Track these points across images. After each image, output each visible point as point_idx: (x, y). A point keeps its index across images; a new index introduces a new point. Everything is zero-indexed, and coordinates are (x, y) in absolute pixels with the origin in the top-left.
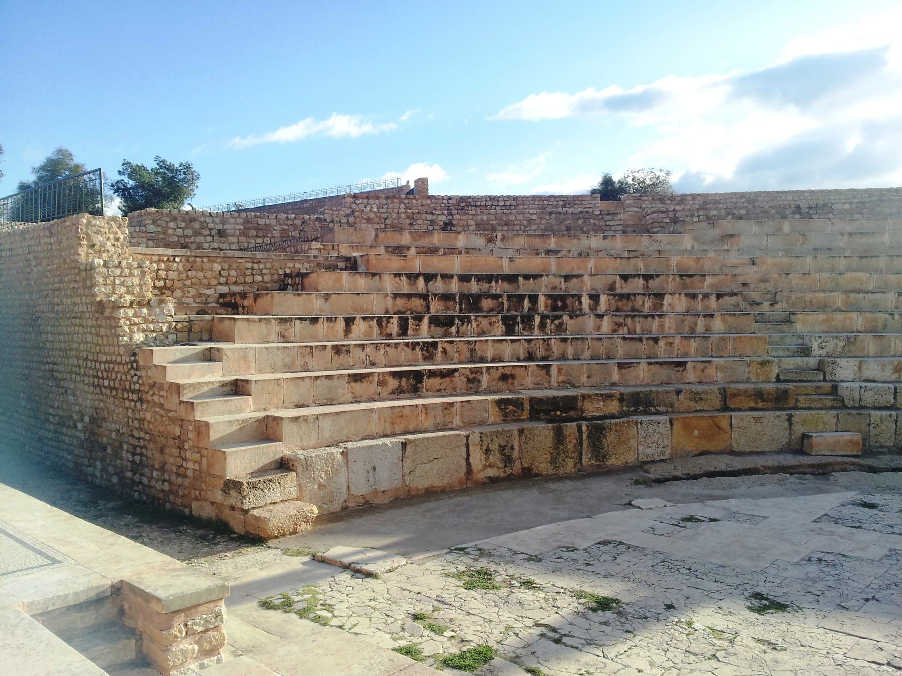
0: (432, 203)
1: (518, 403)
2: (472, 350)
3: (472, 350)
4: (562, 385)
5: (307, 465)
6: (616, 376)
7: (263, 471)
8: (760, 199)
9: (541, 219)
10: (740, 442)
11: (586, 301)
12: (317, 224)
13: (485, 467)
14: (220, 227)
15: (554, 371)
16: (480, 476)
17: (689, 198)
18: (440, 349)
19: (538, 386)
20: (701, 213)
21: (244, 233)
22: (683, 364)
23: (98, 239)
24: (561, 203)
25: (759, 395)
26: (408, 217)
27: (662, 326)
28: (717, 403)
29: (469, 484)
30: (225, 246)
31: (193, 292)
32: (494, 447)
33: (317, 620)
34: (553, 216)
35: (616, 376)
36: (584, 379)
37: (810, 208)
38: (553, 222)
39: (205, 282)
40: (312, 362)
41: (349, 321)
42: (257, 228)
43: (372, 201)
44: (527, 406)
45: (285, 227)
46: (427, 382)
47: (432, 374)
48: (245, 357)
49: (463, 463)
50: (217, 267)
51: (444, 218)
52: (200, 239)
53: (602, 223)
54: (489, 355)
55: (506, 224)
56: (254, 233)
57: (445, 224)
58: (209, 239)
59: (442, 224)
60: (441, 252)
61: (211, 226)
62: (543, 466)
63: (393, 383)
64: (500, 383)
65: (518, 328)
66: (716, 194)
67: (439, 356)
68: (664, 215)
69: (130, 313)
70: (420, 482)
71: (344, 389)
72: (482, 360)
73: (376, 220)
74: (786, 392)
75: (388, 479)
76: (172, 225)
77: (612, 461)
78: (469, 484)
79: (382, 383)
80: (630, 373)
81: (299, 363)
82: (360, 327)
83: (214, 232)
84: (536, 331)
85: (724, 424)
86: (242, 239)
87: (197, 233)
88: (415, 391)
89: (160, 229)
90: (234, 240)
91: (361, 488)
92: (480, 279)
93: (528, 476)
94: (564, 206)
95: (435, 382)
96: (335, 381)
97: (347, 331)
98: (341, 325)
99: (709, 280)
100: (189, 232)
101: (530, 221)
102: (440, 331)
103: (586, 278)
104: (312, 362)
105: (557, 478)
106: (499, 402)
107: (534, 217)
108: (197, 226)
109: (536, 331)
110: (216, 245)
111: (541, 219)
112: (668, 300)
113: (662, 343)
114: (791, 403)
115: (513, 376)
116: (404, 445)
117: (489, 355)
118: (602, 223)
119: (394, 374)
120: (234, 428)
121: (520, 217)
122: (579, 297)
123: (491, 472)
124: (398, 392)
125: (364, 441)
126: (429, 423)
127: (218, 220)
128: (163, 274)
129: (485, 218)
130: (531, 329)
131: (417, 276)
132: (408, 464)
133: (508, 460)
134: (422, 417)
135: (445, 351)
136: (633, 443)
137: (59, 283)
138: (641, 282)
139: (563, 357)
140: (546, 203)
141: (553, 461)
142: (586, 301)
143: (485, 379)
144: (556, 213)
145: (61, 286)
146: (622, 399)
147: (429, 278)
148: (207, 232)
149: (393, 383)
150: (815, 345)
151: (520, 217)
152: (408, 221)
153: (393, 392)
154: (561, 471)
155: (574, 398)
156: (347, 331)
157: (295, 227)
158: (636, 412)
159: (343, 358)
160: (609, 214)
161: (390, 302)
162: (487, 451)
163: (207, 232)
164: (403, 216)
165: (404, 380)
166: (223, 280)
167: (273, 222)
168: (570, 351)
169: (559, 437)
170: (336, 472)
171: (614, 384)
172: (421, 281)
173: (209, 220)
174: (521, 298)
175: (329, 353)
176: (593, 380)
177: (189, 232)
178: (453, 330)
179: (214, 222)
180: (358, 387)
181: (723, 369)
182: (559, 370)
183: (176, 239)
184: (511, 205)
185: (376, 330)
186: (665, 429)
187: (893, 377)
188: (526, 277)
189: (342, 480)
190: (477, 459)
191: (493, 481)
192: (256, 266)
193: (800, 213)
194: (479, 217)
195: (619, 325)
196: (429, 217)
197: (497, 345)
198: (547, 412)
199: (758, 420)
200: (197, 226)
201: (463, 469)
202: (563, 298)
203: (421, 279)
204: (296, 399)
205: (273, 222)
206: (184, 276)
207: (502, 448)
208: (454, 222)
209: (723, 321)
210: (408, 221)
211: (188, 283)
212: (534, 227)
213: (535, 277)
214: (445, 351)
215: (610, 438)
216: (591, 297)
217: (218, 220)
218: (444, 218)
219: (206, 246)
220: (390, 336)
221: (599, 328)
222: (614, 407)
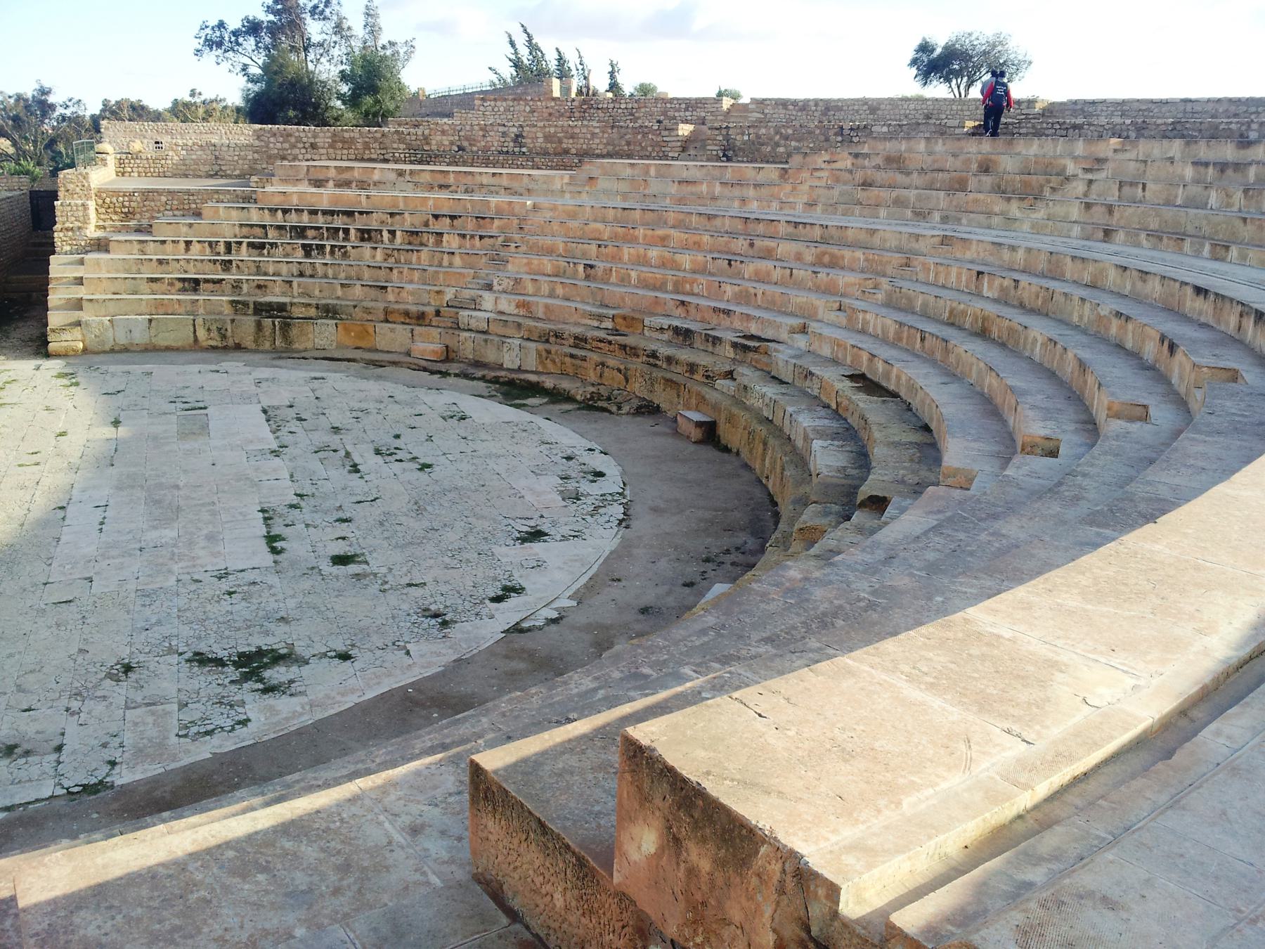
1: (245, 304)
2: (258, 267)
3: (258, 267)
4: (301, 295)
5: (87, 324)
6: (339, 293)
7: (70, 325)
8: (883, 107)
10: (381, 343)
11: (386, 235)
12: (396, 137)
14: (312, 140)
15: (295, 285)
16: (205, 344)
17: (812, 104)
19: (284, 294)
20: (751, 131)
21: (332, 146)
22: (385, 288)
23: (71, 187)
24: (683, 106)
25: (407, 314)
26: (481, 129)
27: (419, 258)
28: (382, 317)
29: (196, 345)
30: (316, 157)
31: (148, 215)
32: (214, 328)
34: (615, 130)
35: (339, 293)
36: (317, 293)
37: (851, 129)
38: (615, 136)
40: (143, 269)
41: (188, 243)
42: (344, 141)
43: (499, 103)
44: (252, 306)
46: (202, 285)
47: (207, 281)
48: (98, 264)
50: (164, 199)
51: (515, 130)
52: (296, 151)
53: (659, 139)
54: (271, 271)
55: (572, 137)
56: (340, 145)
57: (517, 136)
58: (303, 151)
61: (305, 140)
62: (248, 342)
63: (179, 285)
65: (314, 253)
66: (839, 100)
67: (234, 269)
68: (717, 132)
69: (61, 234)
70: (164, 340)
71: (145, 286)
72: (266, 274)
74: (423, 313)
75: (140, 337)
76: (272, 140)
77: (296, 346)
78: (196, 345)
79: (171, 284)
80: (349, 291)
81: (134, 269)
82: (195, 248)
84: (328, 256)
85: (371, 330)
86: (331, 151)
87: (293, 146)
88: (195, 290)
90: (324, 151)
91: (122, 340)
92: (325, 213)
93: (238, 347)
94: (686, 109)
95: (210, 286)
97: (187, 249)
98: (182, 245)
99: (497, 222)
100: (286, 145)
101: (593, 134)
102: (256, 252)
103: (406, 215)
104: (143, 269)
105: (256, 351)
106: (232, 302)
107: (597, 131)
108: (293, 140)
109: (328, 256)
110: (309, 156)
112: (445, 237)
113: (395, 271)
114: (427, 322)
115: (266, 287)
116: (150, 321)
117: (271, 271)
118: (659, 139)
119: (179, 279)
120: (63, 302)
121: (584, 130)
122: (381, 231)
124: (183, 290)
126: (182, 310)
128: (126, 204)
129: (552, 130)
130: (324, 254)
131: (276, 210)
132: (153, 332)
133: (224, 337)
134: (177, 306)
135: (238, 267)
136: (310, 336)
138: (448, 220)
139: (326, 276)
141: (256, 341)
142: (386, 235)
143: (245, 287)
146: (317, 308)
147: (285, 211)
150: (495, 283)
151: (584, 130)
152: (481, 133)
154: (261, 348)
155: (285, 304)
156: (187, 249)
157: (376, 140)
158: (326, 317)
159: (164, 267)
161: (237, 228)
162: (209, 330)
164: (476, 128)
167: (357, 135)
168: (330, 272)
169: (259, 326)
170: (106, 330)
171: (338, 298)
172: (280, 213)
174: (337, 230)
175: (155, 264)
176: (324, 294)
177: (286, 145)
178: (265, 251)
180: (154, 285)
181: (412, 293)
182: (299, 285)
185: (208, 250)
186: (332, 329)
187: (515, 312)
188: (361, 213)
189: (110, 334)
190: (202, 334)
191: (214, 348)
193: (842, 135)
195: (389, 256)
196: (501, 129)
198: (267, 311)
199: (392, 330)
201: (192, 339)
202: (369, 231)
203: (280, 212)
204: (113, 290)
205: (357, 135)
207: (219, 329)
209: (462, 259)
210: (481, 133)
212: (597, 141)
213: (367, 213)
214: (238, 267)
215: (294, 332)
216: (389, 232)
218: (515, 130)
219: (300, 157)
220: (218, 254)
221: (374, 257)
222: (312, 312)
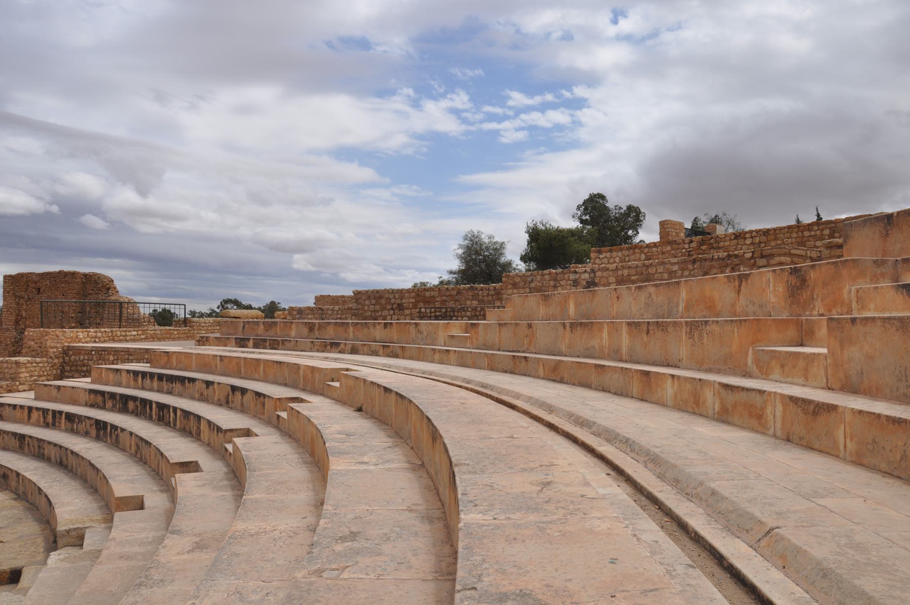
0: (672, 249)
9: (683, 270)
14: (399, 301)
45: (444, 298)
59: (584, 283)
60: (251, 343)
73: (522, 284)
76: (367, 302)
83: (395, 306)
89: (360, 307)
107: (676, 268)
111: (683, 270)
125: (736, 384)
127: (397, 296)
137: (88, 360)
140: (806, 233)
144: (701, 260)
148: (389, 307)
152: (552, 283)
160: (762, 257)
163: (389, 307)
169: (341, 453)
173: (391, 296)
177: (378, 307)
179: (394, 297)
183: (370, 313)
184: (760, 242)
194: (620, 273)
200: (383, 301)
208: (596, 281)
210: (552, 283)
217: (397, 296)
218: (587, 276)
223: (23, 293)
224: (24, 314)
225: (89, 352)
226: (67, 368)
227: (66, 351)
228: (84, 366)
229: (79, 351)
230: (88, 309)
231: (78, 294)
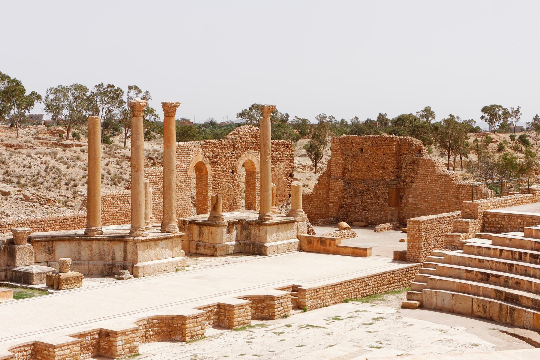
13: (478, 311)
18: (514, 267)
32: (481, 305)
33: (327, 306)
39: (515, 226)
44: (504, 294)
49: (471, 307)
63: (480, 276)
64: (516, 285)
96: (461, 271)
115: (520, 283)
123: (480, 314)
133: (485, 311)
145: (79, 262)
149: (480, 276)
153: (480, 279)
162: (479, 306)
165: (483, 276)
166: (521, 226)
192: (534, 221)
197: (534, 270)
206: (507, 223)
211: (509, 226)
223: (349, 152)
224: (349, 167)
225: (503, 216)
226: (487, 225)
227: (486, 215)
228: (498, 224)
229: (495, 215)
230: (404, 166)
231: (395, 154)
